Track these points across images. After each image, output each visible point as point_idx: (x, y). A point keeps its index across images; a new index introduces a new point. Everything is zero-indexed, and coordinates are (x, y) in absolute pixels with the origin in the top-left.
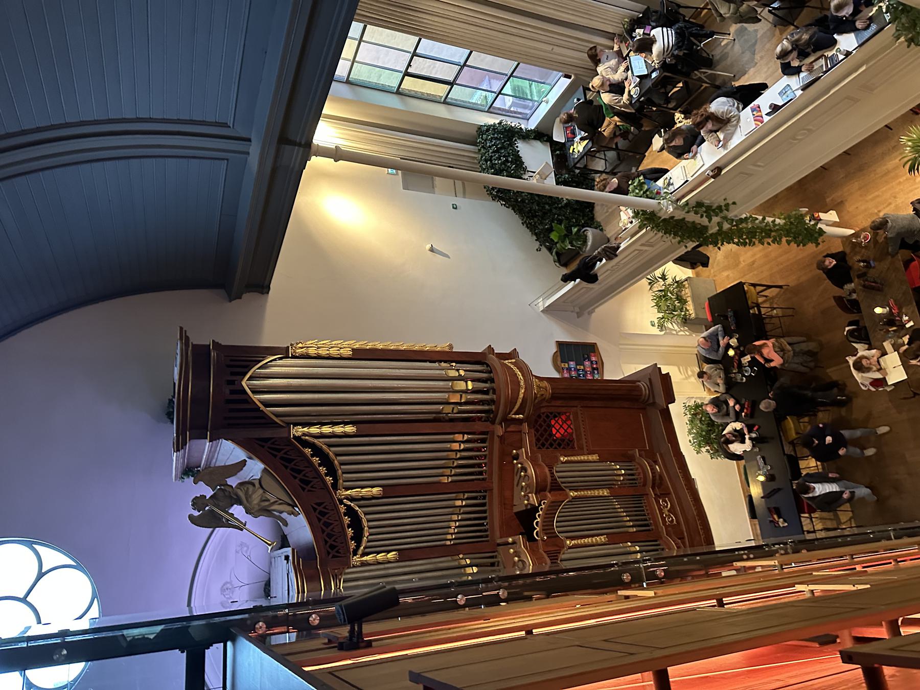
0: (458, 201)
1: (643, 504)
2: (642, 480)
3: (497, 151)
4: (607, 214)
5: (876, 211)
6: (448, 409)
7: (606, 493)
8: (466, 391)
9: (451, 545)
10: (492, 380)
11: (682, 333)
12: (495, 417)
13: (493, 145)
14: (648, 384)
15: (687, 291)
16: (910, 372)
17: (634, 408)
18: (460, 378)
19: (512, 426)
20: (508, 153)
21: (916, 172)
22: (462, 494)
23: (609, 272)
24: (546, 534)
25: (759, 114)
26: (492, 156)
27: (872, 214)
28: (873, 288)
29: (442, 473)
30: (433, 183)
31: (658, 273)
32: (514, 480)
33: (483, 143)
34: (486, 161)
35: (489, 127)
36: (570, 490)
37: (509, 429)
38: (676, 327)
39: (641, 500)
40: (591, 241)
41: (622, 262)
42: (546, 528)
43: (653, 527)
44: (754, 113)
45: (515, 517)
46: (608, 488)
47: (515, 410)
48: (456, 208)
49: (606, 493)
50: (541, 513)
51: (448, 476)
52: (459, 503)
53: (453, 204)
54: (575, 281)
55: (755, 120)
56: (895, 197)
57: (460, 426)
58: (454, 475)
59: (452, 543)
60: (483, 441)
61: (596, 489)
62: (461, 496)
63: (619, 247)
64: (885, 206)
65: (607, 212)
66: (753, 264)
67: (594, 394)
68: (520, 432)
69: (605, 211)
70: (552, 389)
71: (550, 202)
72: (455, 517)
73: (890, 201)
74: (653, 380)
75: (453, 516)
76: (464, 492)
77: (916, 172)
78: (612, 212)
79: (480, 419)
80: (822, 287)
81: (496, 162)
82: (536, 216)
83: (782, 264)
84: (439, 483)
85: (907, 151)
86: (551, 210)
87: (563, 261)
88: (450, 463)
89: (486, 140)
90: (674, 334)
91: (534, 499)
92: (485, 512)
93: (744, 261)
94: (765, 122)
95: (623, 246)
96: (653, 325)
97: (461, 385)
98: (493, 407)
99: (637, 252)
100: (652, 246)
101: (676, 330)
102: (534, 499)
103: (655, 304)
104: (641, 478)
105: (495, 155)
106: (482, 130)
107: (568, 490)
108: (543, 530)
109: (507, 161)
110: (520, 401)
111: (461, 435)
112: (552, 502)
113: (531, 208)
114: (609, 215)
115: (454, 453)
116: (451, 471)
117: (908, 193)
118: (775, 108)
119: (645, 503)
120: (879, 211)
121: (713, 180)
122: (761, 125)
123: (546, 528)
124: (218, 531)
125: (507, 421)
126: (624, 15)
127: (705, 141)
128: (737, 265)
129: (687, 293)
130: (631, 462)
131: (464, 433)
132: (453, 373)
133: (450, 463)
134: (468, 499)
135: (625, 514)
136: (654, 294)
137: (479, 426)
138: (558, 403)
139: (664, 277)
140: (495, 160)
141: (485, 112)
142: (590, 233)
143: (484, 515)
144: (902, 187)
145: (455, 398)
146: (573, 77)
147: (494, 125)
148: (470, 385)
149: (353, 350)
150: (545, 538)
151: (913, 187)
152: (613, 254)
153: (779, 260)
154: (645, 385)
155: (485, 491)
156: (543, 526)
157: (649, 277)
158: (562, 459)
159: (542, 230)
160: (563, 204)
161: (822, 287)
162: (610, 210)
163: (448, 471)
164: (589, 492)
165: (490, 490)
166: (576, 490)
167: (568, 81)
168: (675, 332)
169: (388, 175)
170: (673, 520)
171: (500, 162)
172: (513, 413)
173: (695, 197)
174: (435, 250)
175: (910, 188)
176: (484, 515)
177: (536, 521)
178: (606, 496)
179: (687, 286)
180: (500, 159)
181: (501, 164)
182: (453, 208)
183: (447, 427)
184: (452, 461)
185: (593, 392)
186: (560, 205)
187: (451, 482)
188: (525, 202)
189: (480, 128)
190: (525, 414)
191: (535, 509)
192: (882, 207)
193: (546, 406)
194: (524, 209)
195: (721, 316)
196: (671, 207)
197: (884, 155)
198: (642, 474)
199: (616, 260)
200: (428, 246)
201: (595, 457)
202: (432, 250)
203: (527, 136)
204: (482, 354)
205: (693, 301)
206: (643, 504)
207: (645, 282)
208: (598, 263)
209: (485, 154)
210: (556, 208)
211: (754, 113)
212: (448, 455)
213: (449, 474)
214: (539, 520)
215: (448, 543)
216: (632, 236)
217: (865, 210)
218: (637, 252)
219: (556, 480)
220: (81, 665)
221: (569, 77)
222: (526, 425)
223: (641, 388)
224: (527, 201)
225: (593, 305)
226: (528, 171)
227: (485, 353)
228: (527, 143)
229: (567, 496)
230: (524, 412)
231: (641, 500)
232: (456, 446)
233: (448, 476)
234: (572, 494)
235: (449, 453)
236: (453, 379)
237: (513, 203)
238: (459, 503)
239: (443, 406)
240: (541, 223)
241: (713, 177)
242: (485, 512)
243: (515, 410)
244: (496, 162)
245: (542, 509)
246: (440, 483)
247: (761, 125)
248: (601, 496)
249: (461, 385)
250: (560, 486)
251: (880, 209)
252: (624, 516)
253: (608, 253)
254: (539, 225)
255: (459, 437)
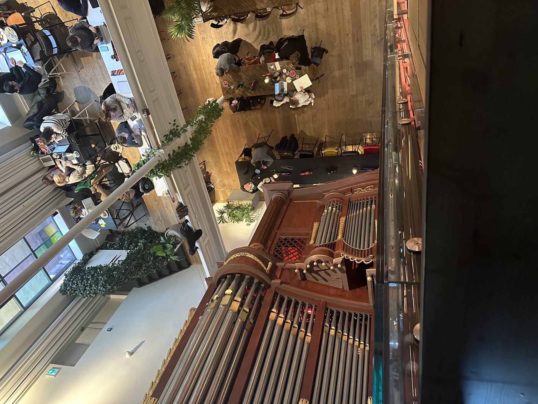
0: (107, 326)
1: (356, 202)
2: (338, 200)
3: (82, 280)
4: (163, 221)
5: (216, 84)
6: (243, 316)
7: (343, 219)
8: (234, 295)
9: (369, 346)
10: (233, 276)
11: (259, 212)
12: (264, 282)
13: (77, 283)
14: (276, 192)
15: (235, 203)
16: (304, 73)
17: (289, 205)
18: (220, 299)
19: (276, 274)
20: (88, 273)
21: (193, 34)
22: (325, 328)
23: (199, 222)
24: (368, 255)
25: (117, 72)
26: (84, 285)
27: (217, 87)
28: (254, 85)
29: (301, 339)
30: (85, 345)
31: (217, 215)
32: (322, 284)
33: (72, 290)
34: (85, 290)
35: (65, 285)
36: (336, 239)
37: (278, 277)
38: (256, 214)
39: (355, 204)
40: (175, 232)
41: (194, 210)
42: (363, 255)
43: (374, 197)
44: (115, 74)
45: (353, 290)
46: (340, 217)
47: (263, 265)
48: (111, 329)
49: (343, 219)
50: (350, 258)
51: (305, 335)
52: (332, 332)
53: (107, 330)
54: (197, 248)
55: (119, 75)
56: (211, 73)
57: (263, 312)
58: (306, 330)
59: (368, 345)
60: (282, 300)
61: (339, 224)
62: (326, 329)
63: (181, 204)
64: (214, 79)
65: (161, 222)
66: (230, 163)
67: (270, 221)
68: (283, 269)
69: (160, 222)
70: (257, 242)
71: (137, 254)
72: (345, 338)
73: (212, 76)
74: (271, 189)
75: (343, 339)
76: (324, 326)
77: (193, 34)
78: (162, 217)
79: (261, 298)
80: (251, 125)
81: (89, 282)
82: (141, 264)
83: (233, 145)
84: (309, 345)
85: (180, 37)
86: (143, 255)
87: (184, 264)
88: (294, 331)
89: (71, 288)
90: (259, 216)
91: (337, 260)
92: (345, 314)
93: (227, 169)
94: (122, 68)
95: (181, 200)
96: (249, 225)
97: (226, 300)
98: (256, 281)
99: (207, 246)
100: (189, 185)
101: (257, 215)
102: (337, 260)
103: (237, 222)
104: (337, 200)
105: (84, 282)
106: (63, 291)
107: (336, 241)
108: (364, 257)
109: (93, 276)
110: (256, 259)
111: (272, 313)
112: (343, 250)
113: (134, 266)
114: (163, 220)
115: (286, 324)
116: (301, 331)
117: (210, 65)
118: (115, 57)
119: (355, 201)
120: (216, 83)
121: (150, 115)
122: (123, 71)
123: (363, 255)
124: (64, 150)
125: (272, 274)
126: (27, 153)
127: (127, 121)
128: (228, 173)
129: (236, 203)
130: (325, 207)
131: (270, 312)
132: (213, 305)
133: (294, 331)
134: (330, 322)
135: (361, 210)
136: (231, 220)
137: (268, 298)
138: (270, 243)
139: (222, 213)
140: (88, 282)
141: (51, 284)
142: (171, 232)
143: (347, 314)
144: (206, 68)
145: (235, 306)
146: (57, 211)
147: (65, 280)
148: (229, 291)
149: (152, 396)
150: (371, 255)
151: (208, 61)
152: (184, 207)
153: (230, 147)
154: (276, 194)
155: (327, 309)
156: (361, 257)
157: (218, 222)
158: (312, 243)
159: (153, 263)
160: (142, 246)
161: (251, 125)
162: (161, 218)
163: (301, 334)
164: (341, 228)
165: (326, 304)
166: (337, 235)
167: (59, 214)
168: (258, 215)
169: (57, 376)
170: (370, 187)
171: (90, 279)
172: (265, 268)
173: (160, 137)
174: (133, 351)
175: (208, 63)
176: (347, 314)
177: (356, 261)
178: (346, 220)
179: (232, 203)
180: (89, 279)
181: (93, 279)
182: (110, 331)
183: (260, 323)
184: (292, 328)
185: (269, 220)
186: (143, 249)
187: (311, 335)
188: (127, 269)
189: (61, 291)
190: (269, 259)
191: (346, 262)
192: (214, 81)
193: (269, 250)
194: (132, 270)
195: (253, 177)
196: (160, 150)
197: (187, 75)
198: (334, 199)
199: (189, 208)
200: (127, 355)
201: (316, 225)
202: (131, 354)
203: (85, 261)
204: (210, 286)
205: (242, 200)
206: (356, 202)
207: (221, 225)
208: (188, 223)
209: (80, 290)
210: (143, 251)
211: (115, 74)
212: (286, 331)
213: (303, 334)
214: (356, 259)
215: (367, 348)
216: (176, 191)
217: (214, 90)
218: (189, 196)
219: (326, 245)
220: (345, 270)
221: (56, 213)
222: (278, 264)
223: (276, 196)
224: (127, 267)
225: (223, 252)
226: (109, 264)
227: (211, 284)
228: (90, 262)
229: (340, 241)
230: (267, 260)
231: (355, 204)
232: (280, 321)
233: (305, 335)
234: (339, 238)
235: (285, 328)
236: (217, 306)
237: (123, 277)
238: (332, 332)
239: (239, 318)
240: (148, 262)
241: (148, 114)
242: (345, 314)
243: (263, 265)
244: (89, 282)
245: (346, 257)
246: (310, 343)
247: (123, 71)
248: (346, 222)
249: (226, 300)
250: (332, 243)
251: (215, 82)
252: (363, 211)
253: (182, 210)
254: (148, 263)
255: (273, 316)
